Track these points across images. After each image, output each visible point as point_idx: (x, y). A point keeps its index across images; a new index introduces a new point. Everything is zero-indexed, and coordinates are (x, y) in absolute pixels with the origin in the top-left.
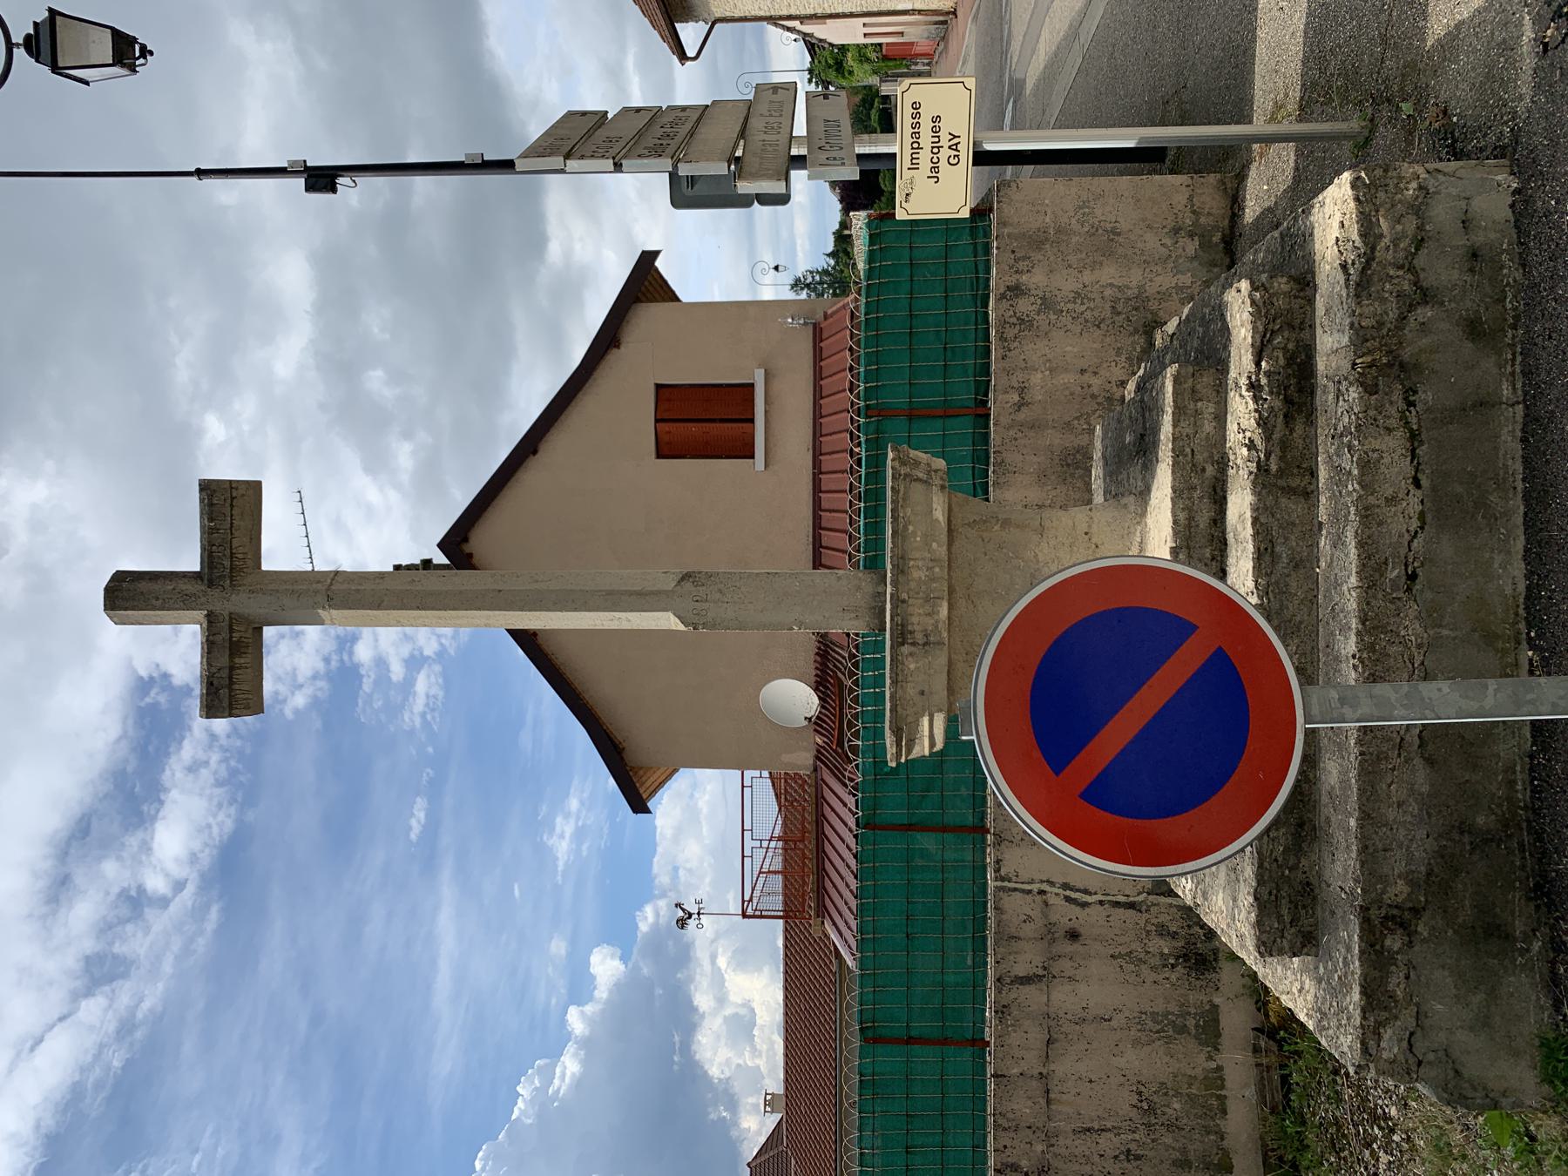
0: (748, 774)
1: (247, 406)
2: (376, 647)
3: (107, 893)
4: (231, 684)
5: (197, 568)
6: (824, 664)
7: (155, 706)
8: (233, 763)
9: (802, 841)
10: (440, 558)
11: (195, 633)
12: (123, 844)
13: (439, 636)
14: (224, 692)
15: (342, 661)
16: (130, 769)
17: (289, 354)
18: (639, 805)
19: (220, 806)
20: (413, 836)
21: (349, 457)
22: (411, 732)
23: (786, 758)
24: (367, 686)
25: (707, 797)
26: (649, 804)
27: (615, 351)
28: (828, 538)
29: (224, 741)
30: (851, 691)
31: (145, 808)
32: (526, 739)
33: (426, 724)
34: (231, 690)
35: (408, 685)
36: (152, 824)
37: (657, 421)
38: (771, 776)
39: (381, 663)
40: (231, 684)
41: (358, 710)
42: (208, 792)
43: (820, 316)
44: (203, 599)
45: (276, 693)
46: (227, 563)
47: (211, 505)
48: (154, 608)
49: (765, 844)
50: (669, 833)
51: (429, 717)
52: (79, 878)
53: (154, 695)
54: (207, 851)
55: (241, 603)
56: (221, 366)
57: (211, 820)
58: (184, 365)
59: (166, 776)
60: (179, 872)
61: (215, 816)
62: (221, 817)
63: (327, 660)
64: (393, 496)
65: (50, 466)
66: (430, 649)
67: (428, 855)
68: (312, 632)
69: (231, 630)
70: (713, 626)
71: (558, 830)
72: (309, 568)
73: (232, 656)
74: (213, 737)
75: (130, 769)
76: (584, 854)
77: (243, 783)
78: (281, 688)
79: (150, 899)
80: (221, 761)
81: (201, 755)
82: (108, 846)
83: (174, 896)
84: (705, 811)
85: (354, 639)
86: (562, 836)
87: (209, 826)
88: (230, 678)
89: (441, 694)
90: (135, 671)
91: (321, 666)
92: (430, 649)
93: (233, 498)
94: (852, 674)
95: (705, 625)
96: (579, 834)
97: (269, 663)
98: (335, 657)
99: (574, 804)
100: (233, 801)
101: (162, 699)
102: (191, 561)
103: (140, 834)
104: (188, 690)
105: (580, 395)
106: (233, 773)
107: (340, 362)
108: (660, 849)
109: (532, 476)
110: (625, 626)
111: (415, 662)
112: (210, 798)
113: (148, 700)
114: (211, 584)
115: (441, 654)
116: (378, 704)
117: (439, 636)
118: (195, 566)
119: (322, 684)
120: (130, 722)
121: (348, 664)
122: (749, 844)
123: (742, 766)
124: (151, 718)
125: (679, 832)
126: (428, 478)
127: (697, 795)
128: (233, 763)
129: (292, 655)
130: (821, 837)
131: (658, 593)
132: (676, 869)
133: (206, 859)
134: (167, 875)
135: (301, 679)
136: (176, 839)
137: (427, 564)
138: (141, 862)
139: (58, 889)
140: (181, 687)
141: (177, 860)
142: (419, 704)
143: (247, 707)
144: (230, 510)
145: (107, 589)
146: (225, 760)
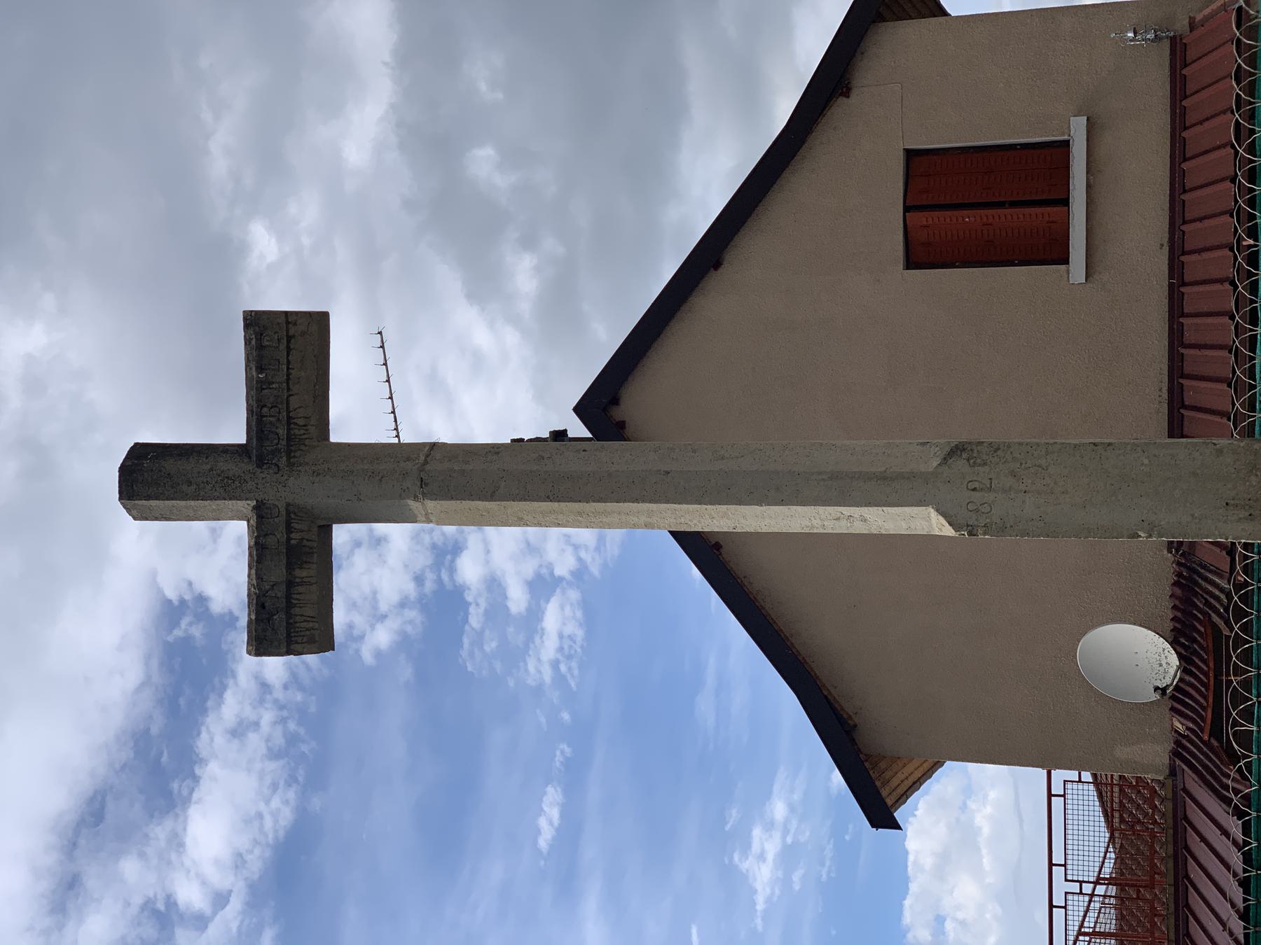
0: (1059, 775)
1: (307, 209)
2: (487, 562)
3: (127, 904)
4: (289, 609)
5: (242, 440)
6: (1187, 601)
7: (187, 640)
8: (292, 726)
9: (1151, 886)
10: (578, 429)
11: (240, 538)
12: (146, 836)
13: (576, 547)
14: (279, 618)
15: (439, 581)
16: (155, 730)
17: (361, 131)
18: (881, 814)
19: (274, 787)
20: (543, 843)
21: (448, 279)
22: (538, 690)
23: (1123, 752)
24: (475, 619)
25: (989, 810)
26: (898, 815)
27: (842, 100)
28: (1195, 391)
29: (279, 694)
30: (1238, 641)
31: (175, 786)
32: (705, 706)
33: (559, 679)
34: (289, 615)
35: (533, 617)
36: (185, 809)
37: (907, 209)
38: (1096, 782)
39: (494, 585)
40: (289, 609)
41: (464, 653)
42: (258, 766)
43: (1182, 25)
44: (251, 485)
45: (351, 626)
46: (282, 432)
47: (260, 347)
48: (185, 497)
49: (1087, 888)
50: (928, 862)
51: (563, 668)
52: (91, 882)
53: (190, 628)
54: (257, 851)
55: (300, 489)
56: (270, 160)
57: (262, 807)
58: (222, 152)
59: (202, 744)
60: (221, 879)
61: (267, 802)
62: (276, 803)
63: (419, 579)
64: (511, 337)
65: (49, 301)
66: (564, 566)
67: (565, 874)
68: (397, 533)
69: (289, 529)
70: (1002, 529)
71: (756, 847)
72: (396, 440)
73: (290, 567)
74: (265, 687)
75: (155, 730)
76: (797, 887)
77: (307, 756)
78: (359, 620)
79: (181, 917)
80: (275, 723)
81: (249, 713)
82: (127, 838)
83: (215, 913)
84: (986, 830)
85: (457, 549)
86: (762, 857)
87: (260, 816)
88: (288, 597)
89: (580, 633)
90: (160, 591)
91: (410, 588)
92: (564, 566)
93: (289, 338)
94: (1239, 614)
95: (987, 529)
96: (788, 856)
97: (340, 581)
98: (430, 576)
99: (779, 809)
100: (292, 780)
101: (197, 632)
102: (234, 431)
103: (169, 823)
104: (229, 620)
105: (786, 174)
106: (292, 740)
107: (433, 136)
108: (914, 887)
109: (714, 303)
110: (859, 528)
111: (543, 585)
112: (261, 778)
113: (178, 633)
114: (261, 462)
115: (580, 574)
116: (491, 645)
117: (576, 547)
118: (242, 440)
119: (412, 614)
120: (155, 663)
121: (449, 586)
122: (1060, 887)
123: (1048, 763)
124: (182, 669)
125: (944, 861)
126: (559, 310)
127: (972, 805)
128: (292, 726)
129: (374, 565)
130: (1182, 883)
131: (912, 476)
132: (940, 920)
133: (255, 865)
134: (204, 883)
135: (383, 607)
136: (217, 831)
137: (559, 435)
138: (169, 863)
139: (65, 895)
140: (222, 616)
141: (217, 862)
142: (549, 648)
143: (312, 641)
144: (286, 353)
145: (123, 469)
146: (282, 721)
